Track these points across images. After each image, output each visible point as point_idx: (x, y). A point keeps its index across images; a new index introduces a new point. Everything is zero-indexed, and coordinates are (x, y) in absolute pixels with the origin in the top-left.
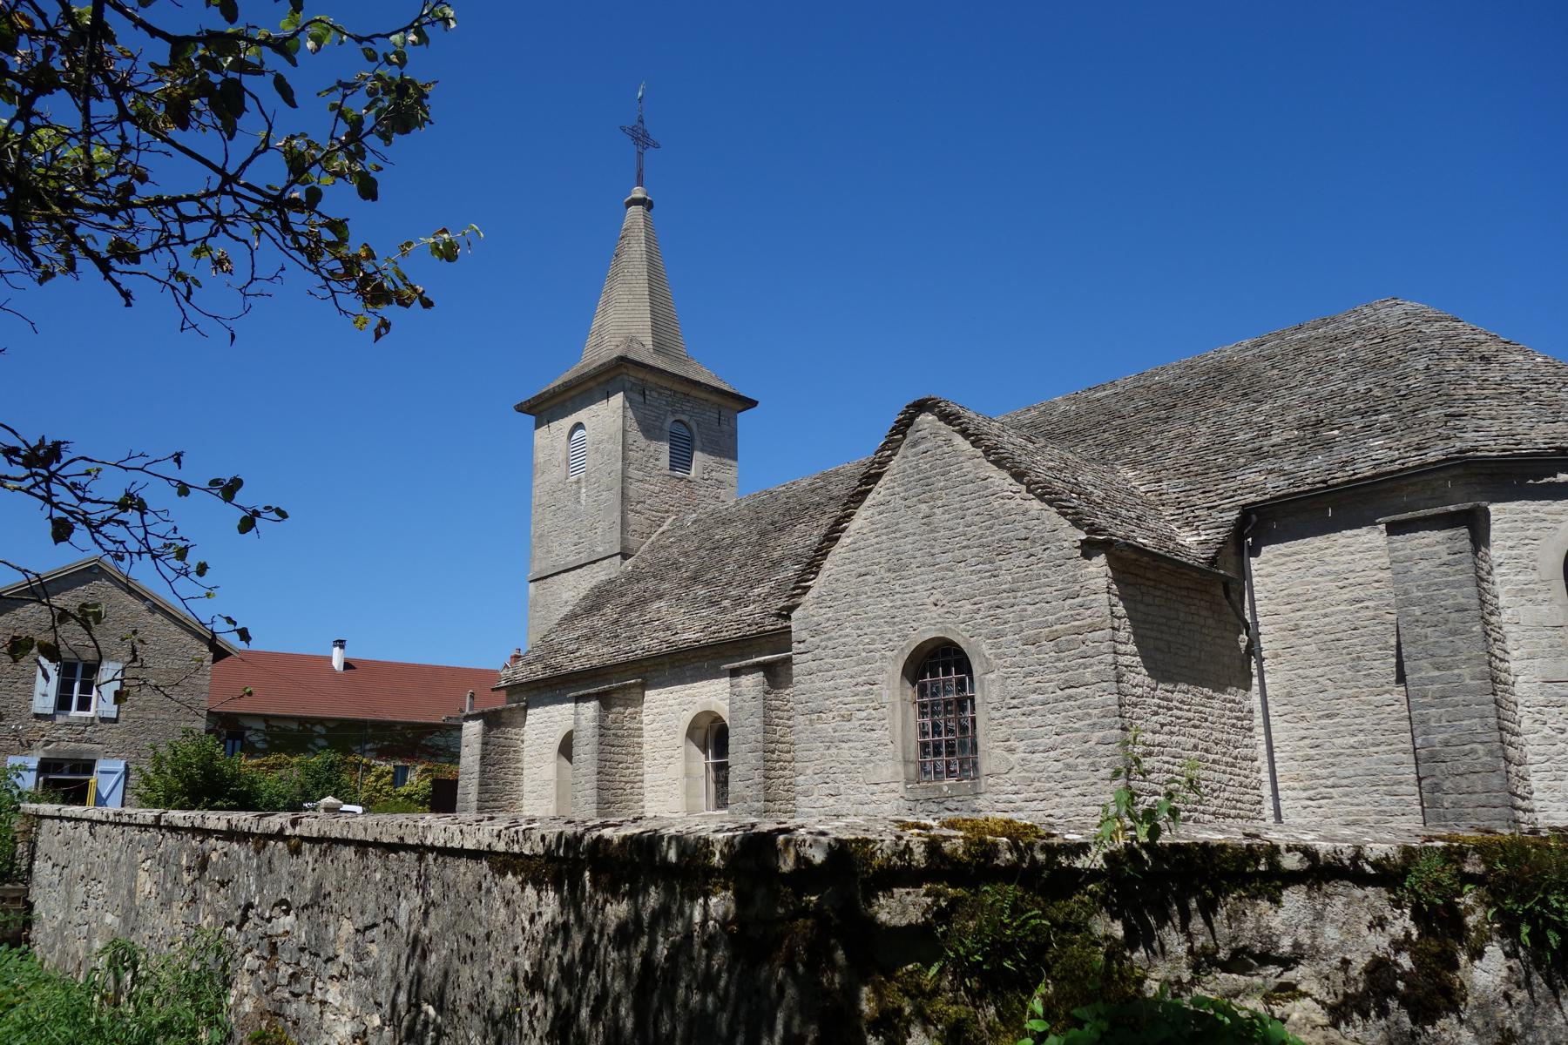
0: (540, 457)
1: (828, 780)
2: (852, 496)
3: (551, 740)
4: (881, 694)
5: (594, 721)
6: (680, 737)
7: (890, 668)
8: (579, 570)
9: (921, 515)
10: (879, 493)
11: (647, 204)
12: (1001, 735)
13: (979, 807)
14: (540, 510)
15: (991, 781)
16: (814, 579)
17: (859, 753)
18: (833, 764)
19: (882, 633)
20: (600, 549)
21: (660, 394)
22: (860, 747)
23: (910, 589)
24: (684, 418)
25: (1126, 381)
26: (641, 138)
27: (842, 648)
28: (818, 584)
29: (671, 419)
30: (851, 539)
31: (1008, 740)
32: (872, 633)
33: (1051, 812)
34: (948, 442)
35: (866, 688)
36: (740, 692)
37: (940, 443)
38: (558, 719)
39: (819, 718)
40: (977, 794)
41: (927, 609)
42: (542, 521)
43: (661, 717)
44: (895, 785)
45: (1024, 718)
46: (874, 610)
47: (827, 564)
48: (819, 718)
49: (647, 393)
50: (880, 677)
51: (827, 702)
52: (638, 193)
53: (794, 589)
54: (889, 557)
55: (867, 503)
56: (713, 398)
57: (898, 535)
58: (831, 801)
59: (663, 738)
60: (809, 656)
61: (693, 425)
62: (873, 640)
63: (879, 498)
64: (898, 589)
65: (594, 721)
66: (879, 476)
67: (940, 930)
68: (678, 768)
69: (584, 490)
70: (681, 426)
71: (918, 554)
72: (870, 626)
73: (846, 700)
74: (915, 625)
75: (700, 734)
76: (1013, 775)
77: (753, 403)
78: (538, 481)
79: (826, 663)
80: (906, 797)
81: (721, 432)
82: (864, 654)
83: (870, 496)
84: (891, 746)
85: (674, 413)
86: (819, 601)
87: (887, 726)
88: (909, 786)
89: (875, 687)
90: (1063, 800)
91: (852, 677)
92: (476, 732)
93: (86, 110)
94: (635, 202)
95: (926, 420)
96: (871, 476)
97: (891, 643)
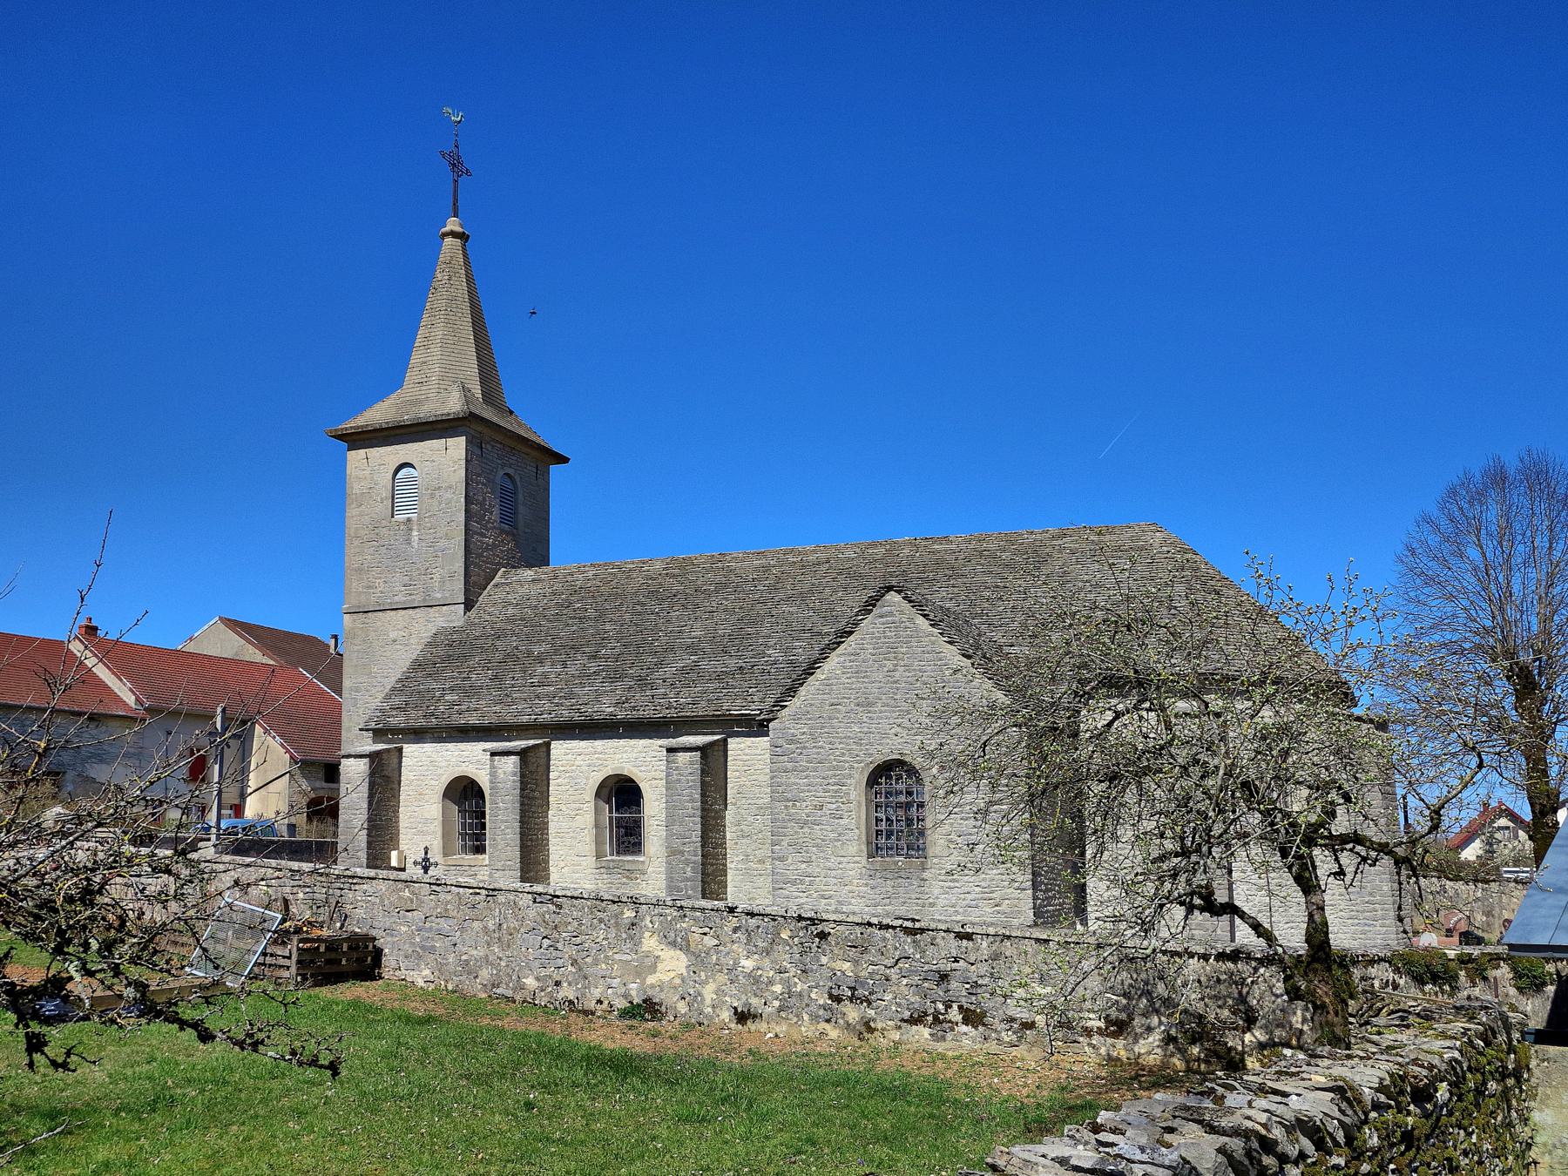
0: (355, 487)
1: (801, 851)
2: (829, 645)
3: (433, 782)
4: (848, 794)
5: (515, 775)
6: (590, 795)
7: (856, 776)
8: (411, 611)
9: (886, 669)
10: (851, 643)
11: (462, 236)
12: (944, 831)
13: (926, 878)
14: (356, 543)
15: (935, 860)
16: (791, 700)
17: (830, 834)
18: (805, 840)
19: (850, 750)
20: (439, 595)
21: (493, 446)
22: (829, 829)
23: (875, 721)
24: (511, 471)
25: (958, 536)
26: (456, 165)
27: (815, 756)
28: (794, 704)
29: (501, 473)
30: (825, 676)
31: (950, 835)
32: (842, 749)
33: (979, 884)
34: (911, 620)
35: (835, 788)
36: (677, 767)
37: (904, 620)
38: (443, 764)
39: (794, 805)
40: (924, 869)
41: (888, 738)
42: (354, 555)
43: (567, 775)
44: (859, 858)
45: (962, 821)
46: (842, 732)
47: (803, 691)
48: (794, 805)
49: (483, 445)
50: (849, 781)
51: (802, 794)
52: (452, 224)
53: (774, 706)
54: (858, 695)
55: (839, 651)
56: (535, 453)
57: (866, 680)
58: (804, 866)
59: (570, 793)
60: (786, 758)
61: (517, 478)
62: (843, 754)
63: (850, 650)
64: (865, 720)
65: (515, 775)
66: (851, 633)
67: (635, 985)
68: (589, 818)
69: (415, 533)
70: (508, 480)
71: (884, 697)
72: (840, 743)
73: (818, 794)
74: (880, 748)
75: (605, 791)
76: (952, 857)
77: (564, 460)
78: (352, 511)
79: (800, 766)
80: (868, 866)
81: (538, 486)
82: (835, 763)
83: (843, 646)
84: (856, 831)
85: (503, 466)
86: (796, 718)
87: (854, 816)
88: (870, 860)
89: (844, 788)
90: (987, 876)
91: (824, 778)
92: (360, 771)
93: (1337, 860)
94: (453, 234)
95: (893, 597)
96: (845, 632)
97: (858, 758)
